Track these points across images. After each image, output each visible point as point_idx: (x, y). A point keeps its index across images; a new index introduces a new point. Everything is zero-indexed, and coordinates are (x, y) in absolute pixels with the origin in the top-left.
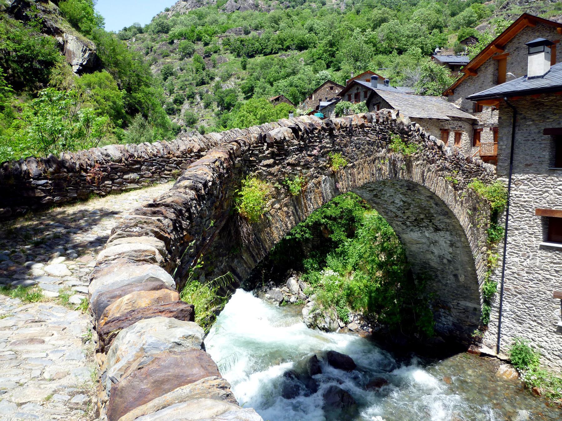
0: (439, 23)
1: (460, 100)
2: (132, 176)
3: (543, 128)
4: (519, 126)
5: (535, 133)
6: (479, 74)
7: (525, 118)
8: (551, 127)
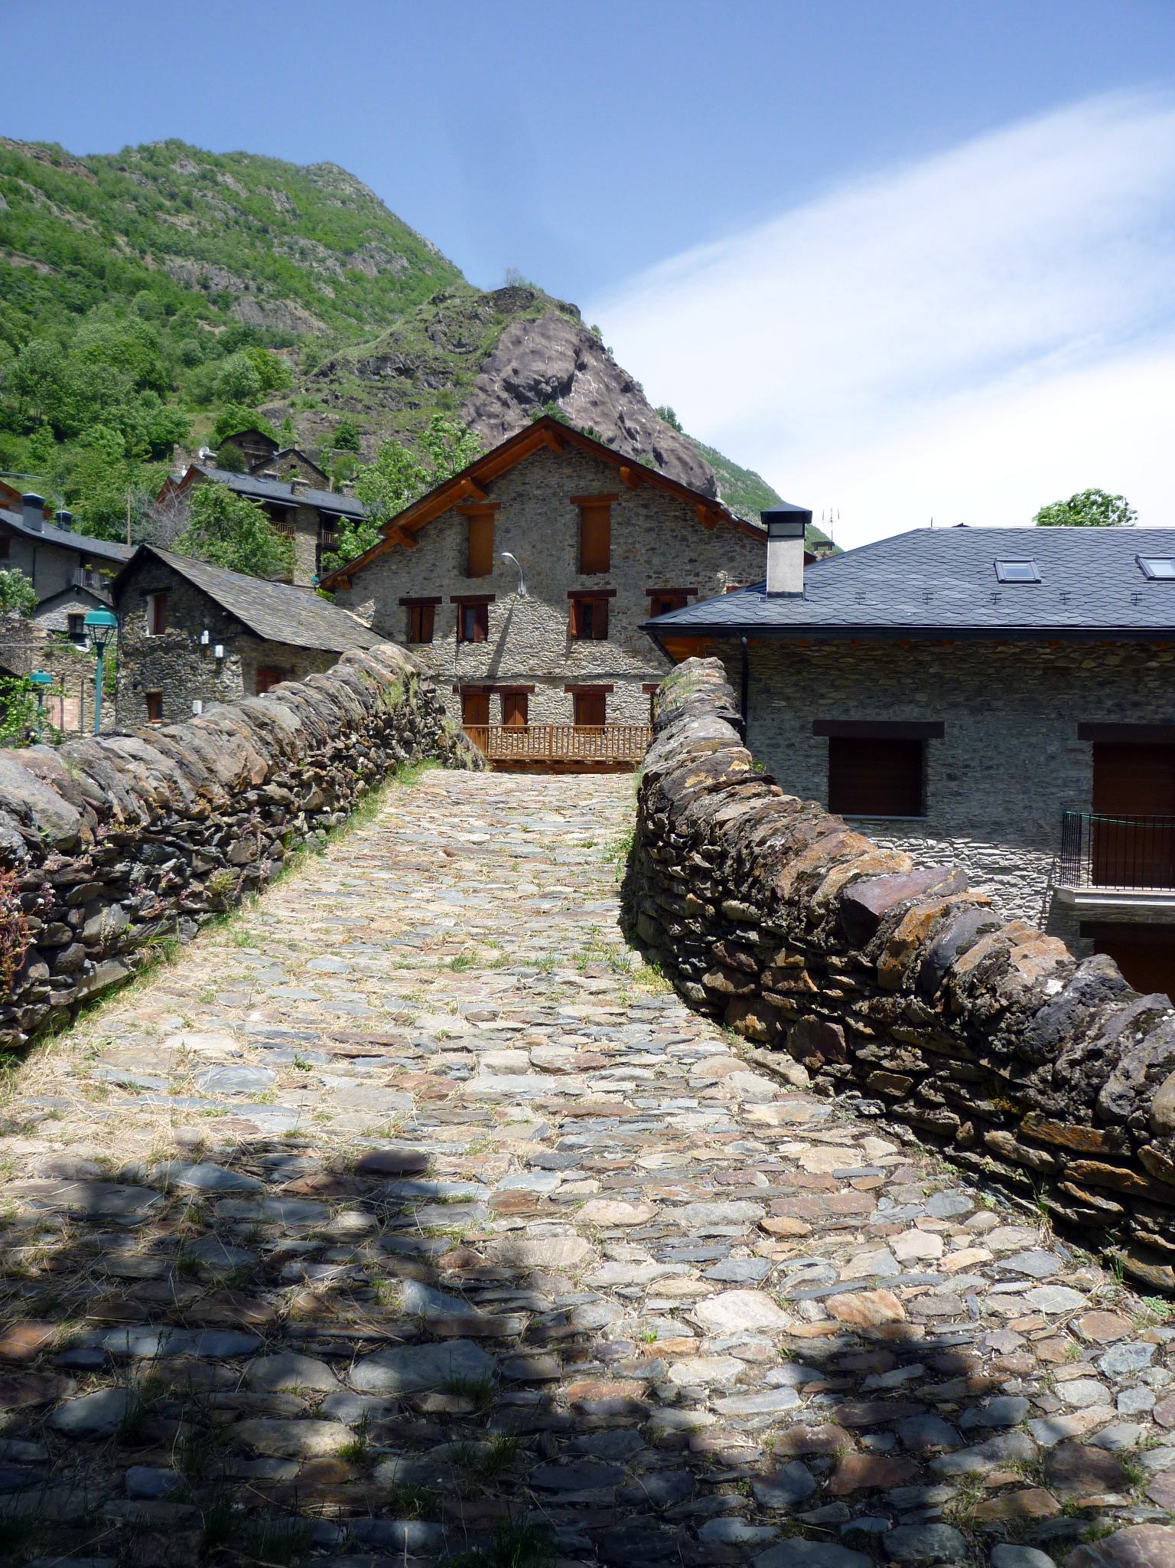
0: (155, 376)
1: (370, 606)
2: (107, 920)
3: (811, 719)
4: (755, 709)
5: (793, 729)
6: (422, 544)
7: (767, 690)
8: (828, 718)
